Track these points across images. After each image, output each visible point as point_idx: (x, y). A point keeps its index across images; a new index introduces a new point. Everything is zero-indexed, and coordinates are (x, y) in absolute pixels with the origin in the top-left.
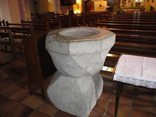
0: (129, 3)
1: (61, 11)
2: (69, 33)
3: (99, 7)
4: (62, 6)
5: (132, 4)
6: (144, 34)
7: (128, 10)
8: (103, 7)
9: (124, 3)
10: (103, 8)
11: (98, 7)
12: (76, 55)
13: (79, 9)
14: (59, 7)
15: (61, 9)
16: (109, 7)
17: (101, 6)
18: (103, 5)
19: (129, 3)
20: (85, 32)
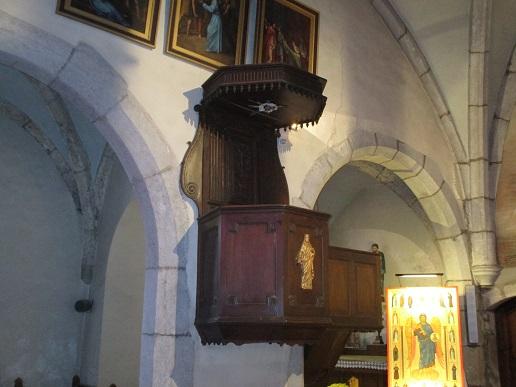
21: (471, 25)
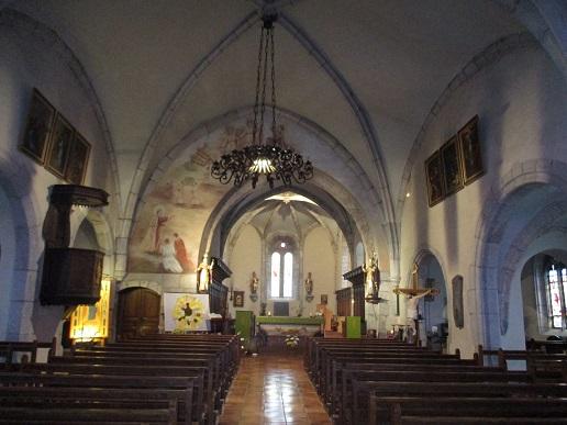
0: (254, 301)
1: (31, 330)
2: (512, 246)
3: (183, 313)
4: (43, 304)
5: (264, 306)
6: (364, 122)
7: (278, 327)
8: (199, 315)
9: (239, 301)
10: (196, 321)
11: (179, 313)
12: (236, 112)
13: (97, 319)
14: (27, 310)
15: (35, 319)
16: (220, 316)
17: (188, 311)
18: (197, 309)
19: (254, 301)
20: (480, 347)
21: (143, 154)
